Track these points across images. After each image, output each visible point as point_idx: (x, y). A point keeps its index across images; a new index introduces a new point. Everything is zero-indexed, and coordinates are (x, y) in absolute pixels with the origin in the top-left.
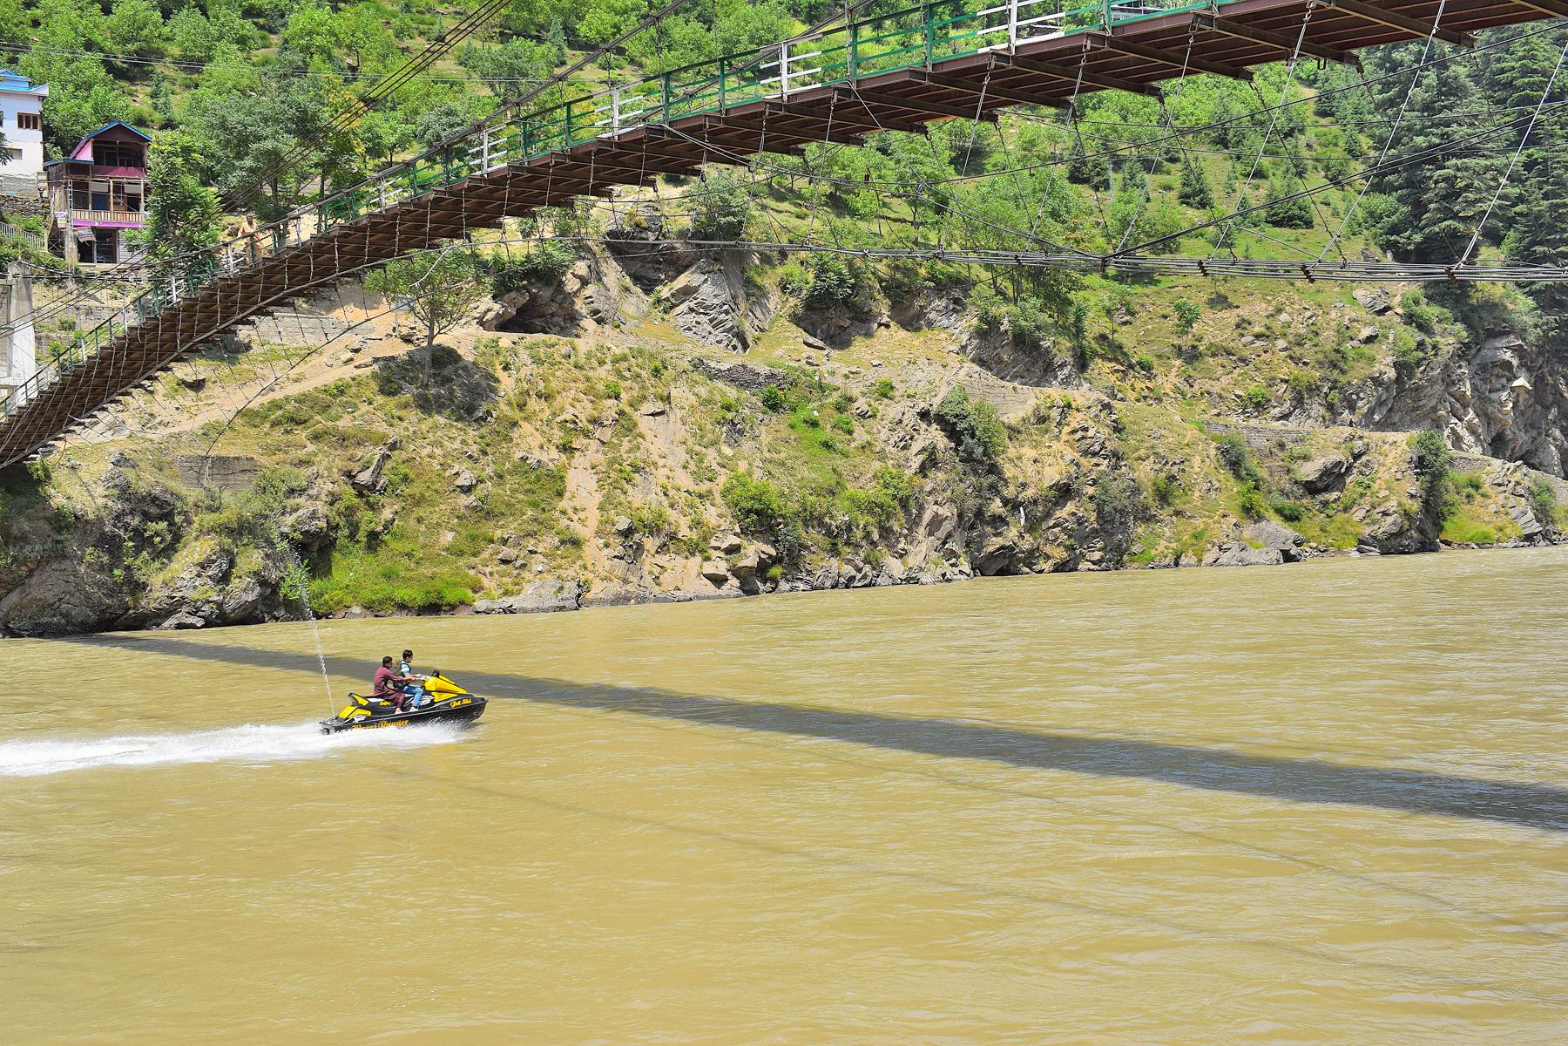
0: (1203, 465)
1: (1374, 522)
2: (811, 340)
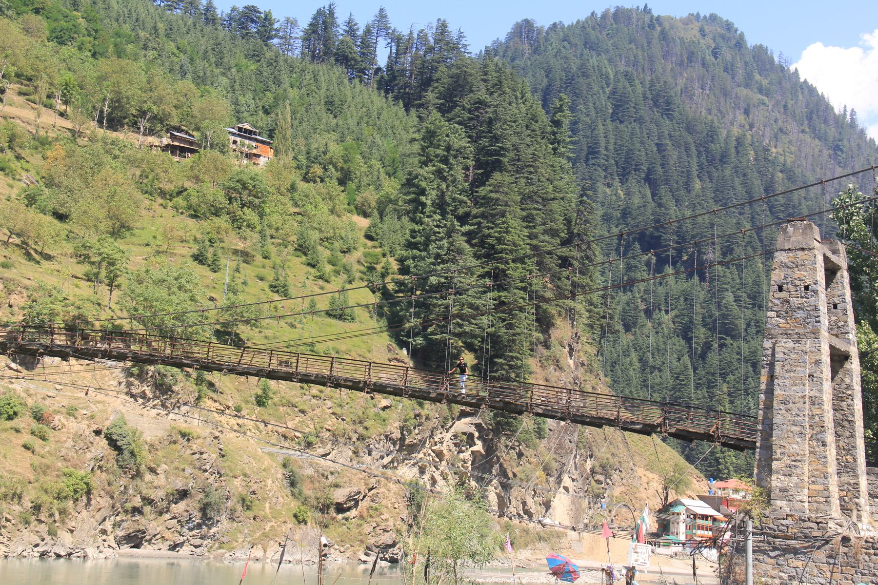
0: (274, 484)
1: (377, 535)
2: (13, 365)
